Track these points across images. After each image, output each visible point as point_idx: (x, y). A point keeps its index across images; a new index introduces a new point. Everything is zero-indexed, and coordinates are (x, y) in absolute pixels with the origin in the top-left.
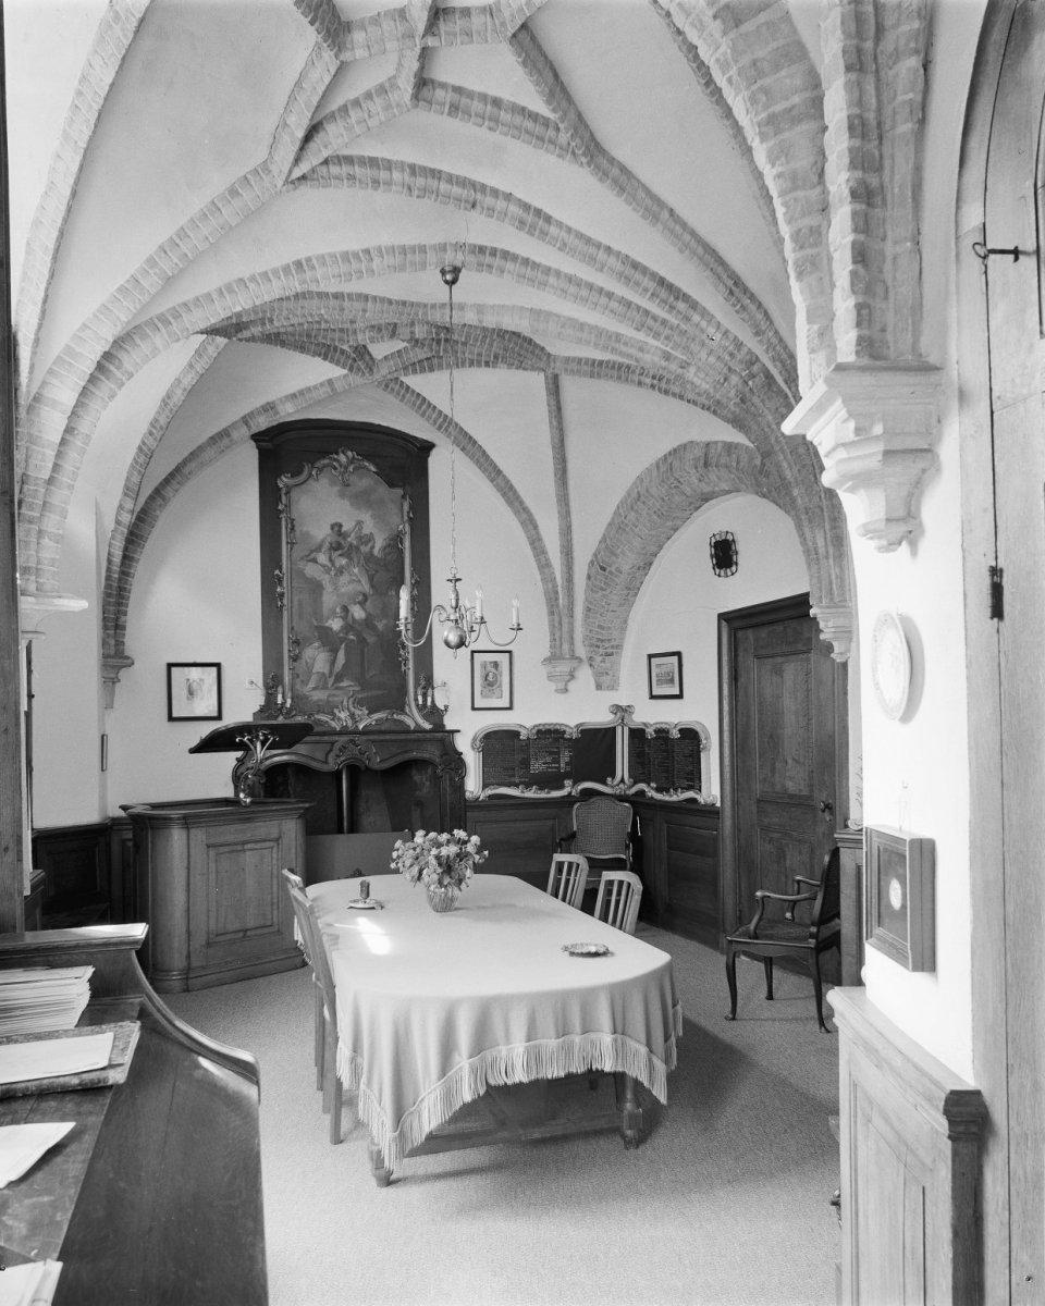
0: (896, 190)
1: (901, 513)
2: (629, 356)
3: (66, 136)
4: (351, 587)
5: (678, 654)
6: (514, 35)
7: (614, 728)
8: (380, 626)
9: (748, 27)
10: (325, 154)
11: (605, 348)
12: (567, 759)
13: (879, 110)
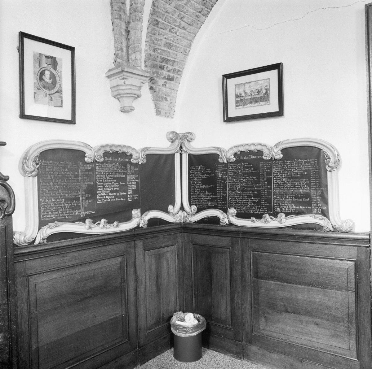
7: (173, 155)
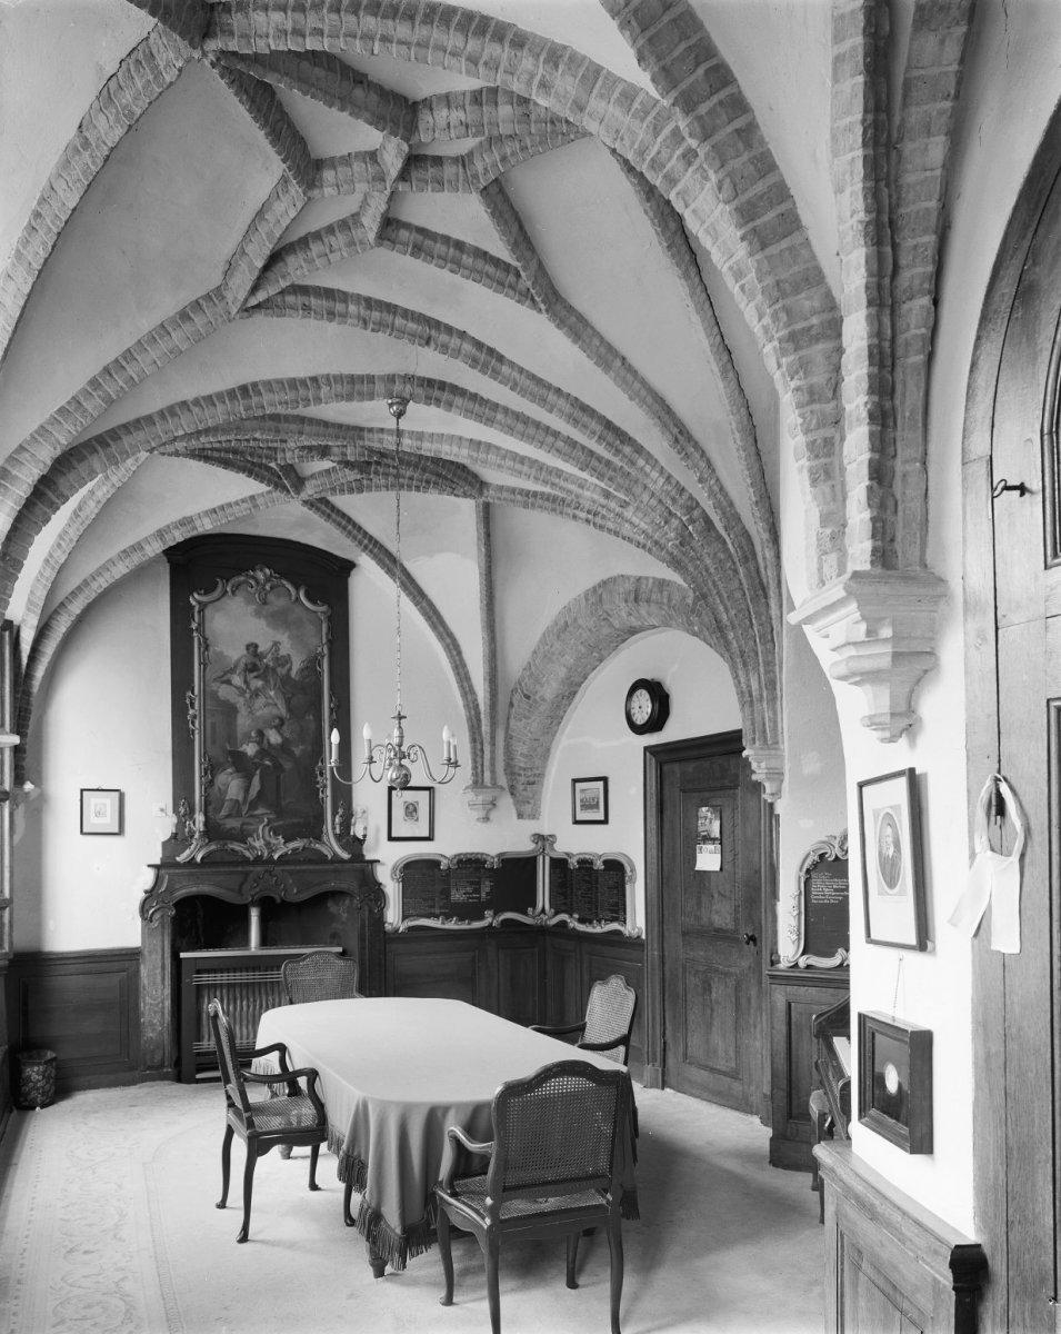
0: (907, 414)
1: (903, 708)
2: (569, 492)
3: (19, 255)
4: (266, 710)
5: (605, 780)
6: (485, 188)
7: (536, 857)
8: (297, 751)
9: (773, 250)
10: (283, 284)
11: (545, 482)
12: (488, 890)
13: (893, 340)
